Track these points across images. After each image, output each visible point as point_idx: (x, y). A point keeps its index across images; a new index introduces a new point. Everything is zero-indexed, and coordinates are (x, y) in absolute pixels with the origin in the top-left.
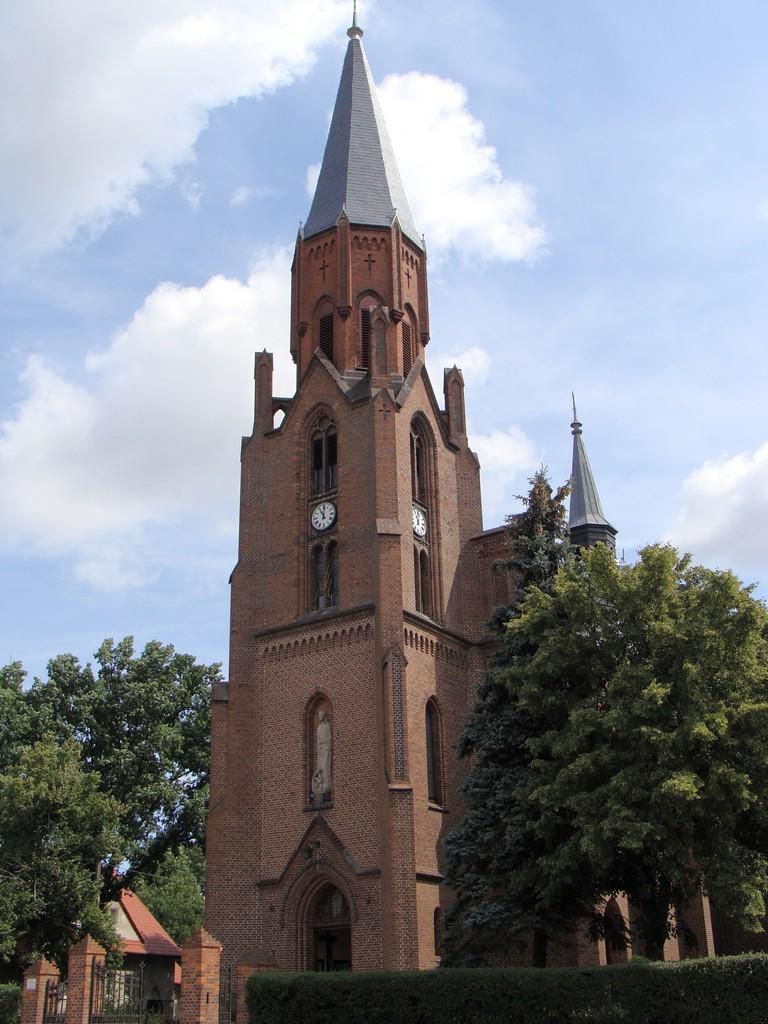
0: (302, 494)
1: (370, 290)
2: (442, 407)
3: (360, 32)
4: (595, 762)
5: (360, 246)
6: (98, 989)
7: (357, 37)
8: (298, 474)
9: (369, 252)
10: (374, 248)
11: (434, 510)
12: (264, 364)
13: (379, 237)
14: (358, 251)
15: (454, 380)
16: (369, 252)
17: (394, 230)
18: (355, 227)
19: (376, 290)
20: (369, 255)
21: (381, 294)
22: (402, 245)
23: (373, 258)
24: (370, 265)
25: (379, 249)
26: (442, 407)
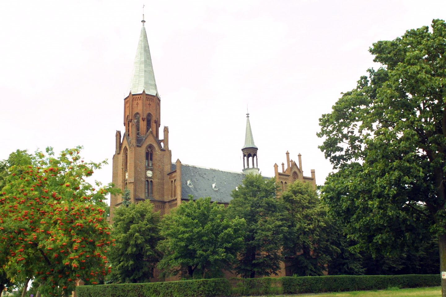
12: (118, 134)
15: (166, 130)
26: (121, 142)
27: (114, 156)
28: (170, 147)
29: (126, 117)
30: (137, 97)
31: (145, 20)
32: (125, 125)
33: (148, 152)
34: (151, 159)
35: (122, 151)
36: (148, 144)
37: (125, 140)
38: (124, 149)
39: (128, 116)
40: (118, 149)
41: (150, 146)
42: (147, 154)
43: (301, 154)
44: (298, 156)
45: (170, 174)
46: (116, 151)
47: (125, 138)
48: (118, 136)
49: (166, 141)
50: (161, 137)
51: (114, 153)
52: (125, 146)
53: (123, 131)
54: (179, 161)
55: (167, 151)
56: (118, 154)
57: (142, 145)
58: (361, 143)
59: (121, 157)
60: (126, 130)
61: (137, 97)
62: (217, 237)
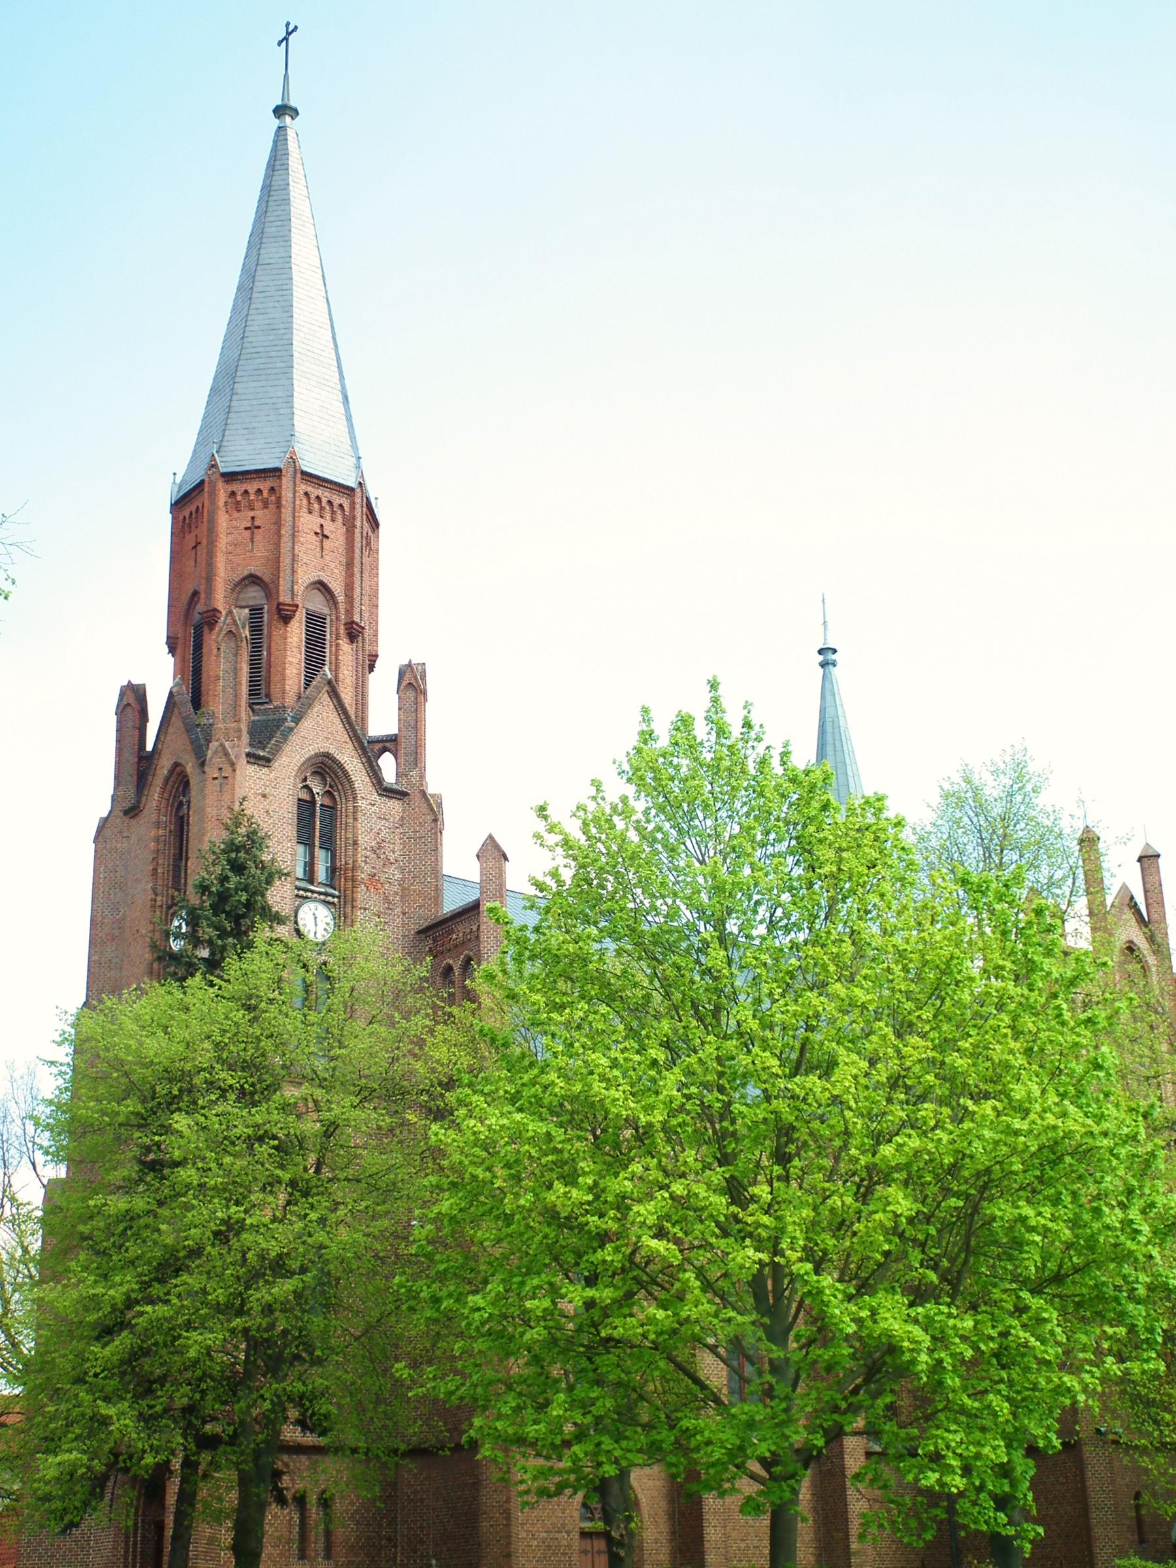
0: (159, 898)
1: (251, 576)
2: (149, 747)
3: (294, 113)
4: (657, 1131)
5: (237, 507)
6: (135, 1544)
7: (288, 119)
8: (155, 869)
9: (252, 514)
10: (258, 505)
11: (349, 898)
12: (132, 701)
13: (264, 486)
14: (236, 514)
15: (412, 683)
16: (252, 514)
17: (358, 490)
18: (308, 477)
19: (259, 574)
20: (253, 518)
21: (266, 579)
22: (302, 487)
23: (257, 523)
24: (322, 541)
25: (266, 506)
26: (149, 747)
27: (104, 824)
28: (434, 784)
29: (185, 599)
30: (252, 487)
31: (292, 103)
32: (172, 650)
33: (305, 796)
34: (329, 844)
35: (154, 796)
36: (311, 750)
37: (171, 730)
38: (167, 780)
39: (196, 593)
40: (131, 792)
41: (325, 767)
42: (306, 808)
43: (1159, 849)
44: (1140, 859)
45: (440, 932)
46: (114, 798)
47: (176, 723)
48: (132, 716)
49: (407, 744)
50: (382, 719)
51: (104, 809)
52: (176, 765)
53: (160, 679)
54: (497, 847)
55: (417, 799)
56: (126, 813)
57: (277, 750)
58: (777, 1383)
59: (148, 830)
60: (179, 670)
61: (252, 491)
62: (933, 1129)
